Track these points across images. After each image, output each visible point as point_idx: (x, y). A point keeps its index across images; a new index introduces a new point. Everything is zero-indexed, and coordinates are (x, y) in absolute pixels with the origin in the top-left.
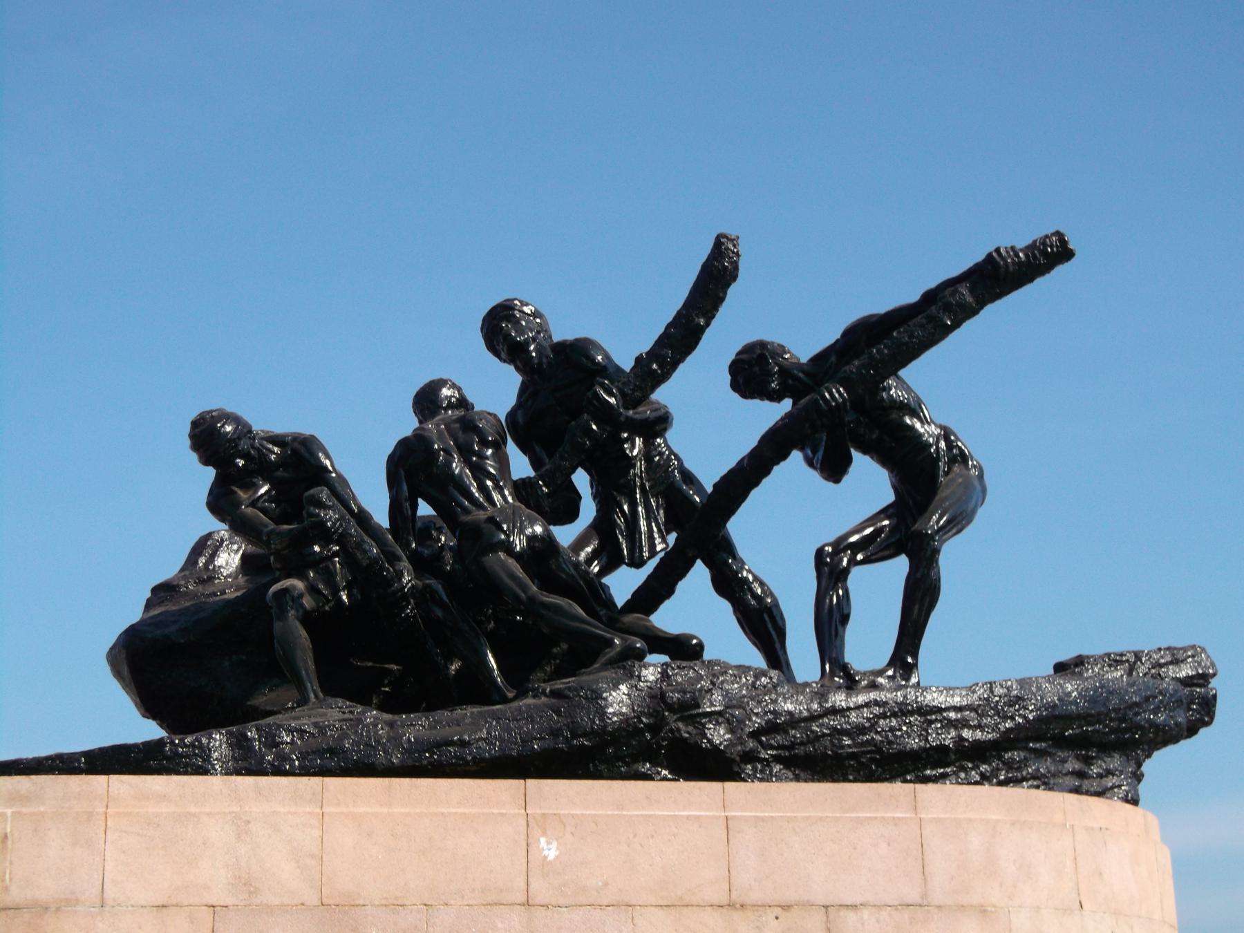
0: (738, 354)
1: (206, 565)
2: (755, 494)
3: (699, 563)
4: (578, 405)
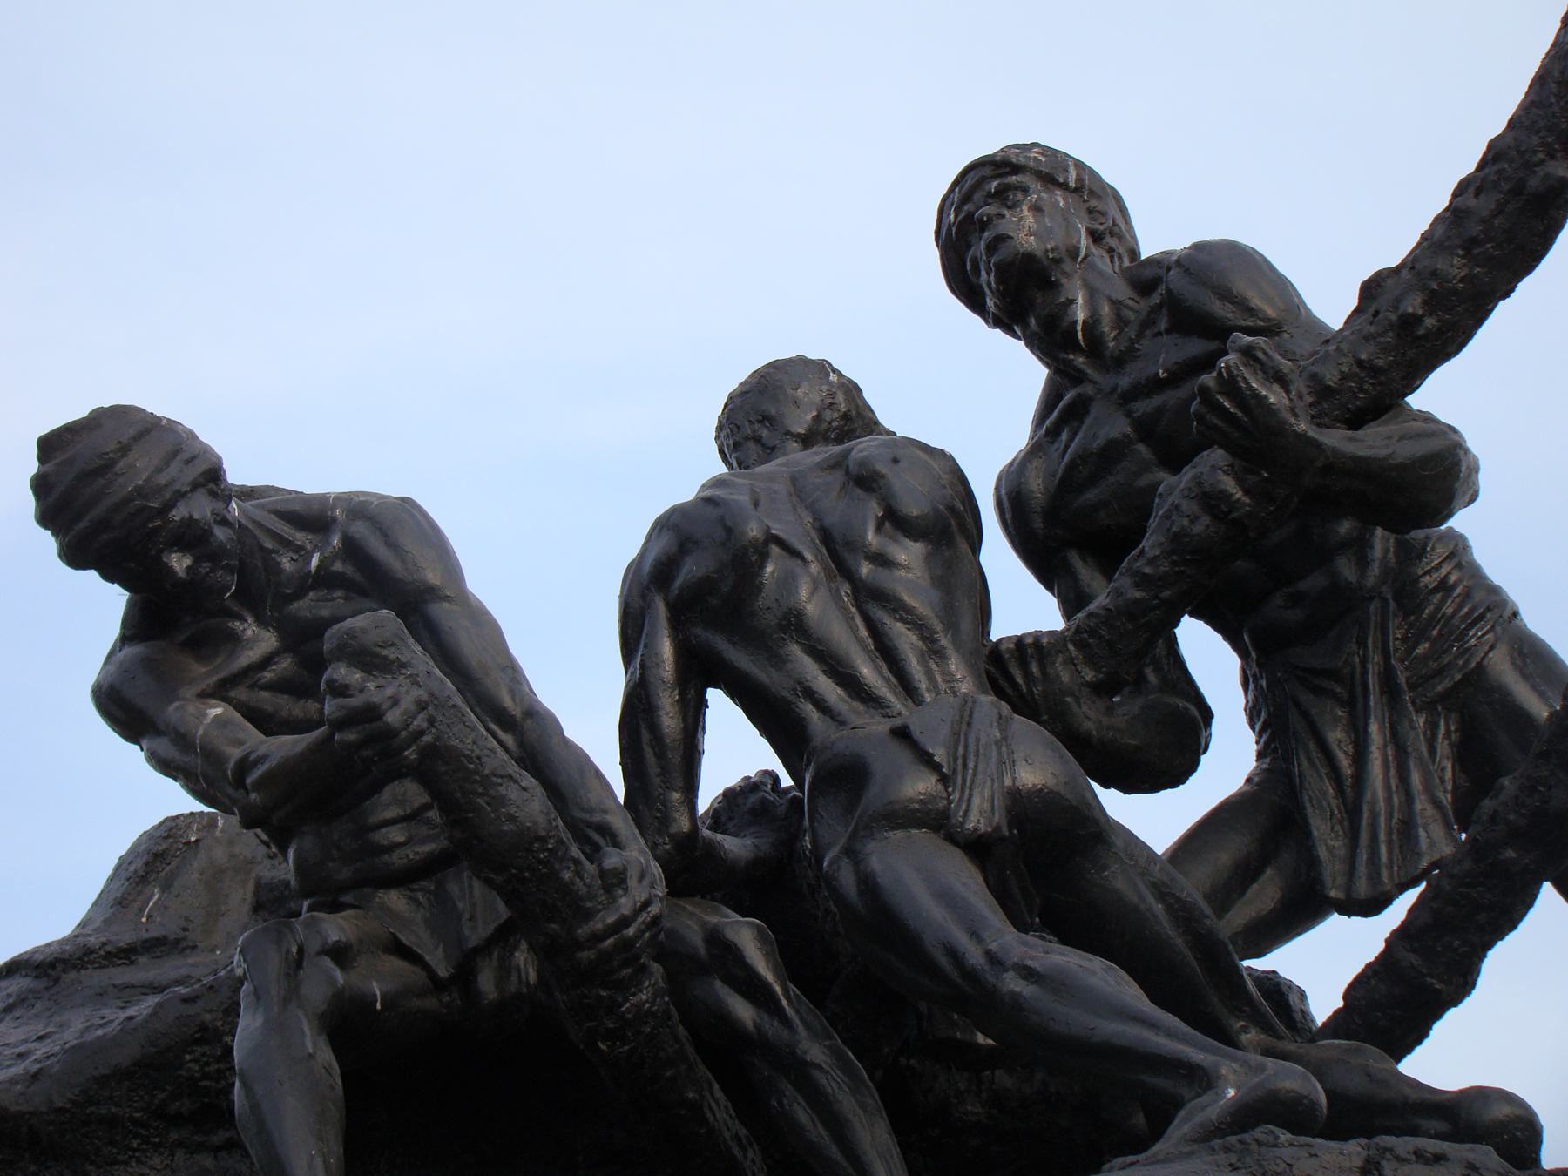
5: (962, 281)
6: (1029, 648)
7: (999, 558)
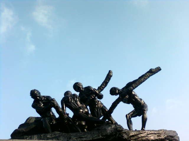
1: (29, 122)
4: (89, 95)
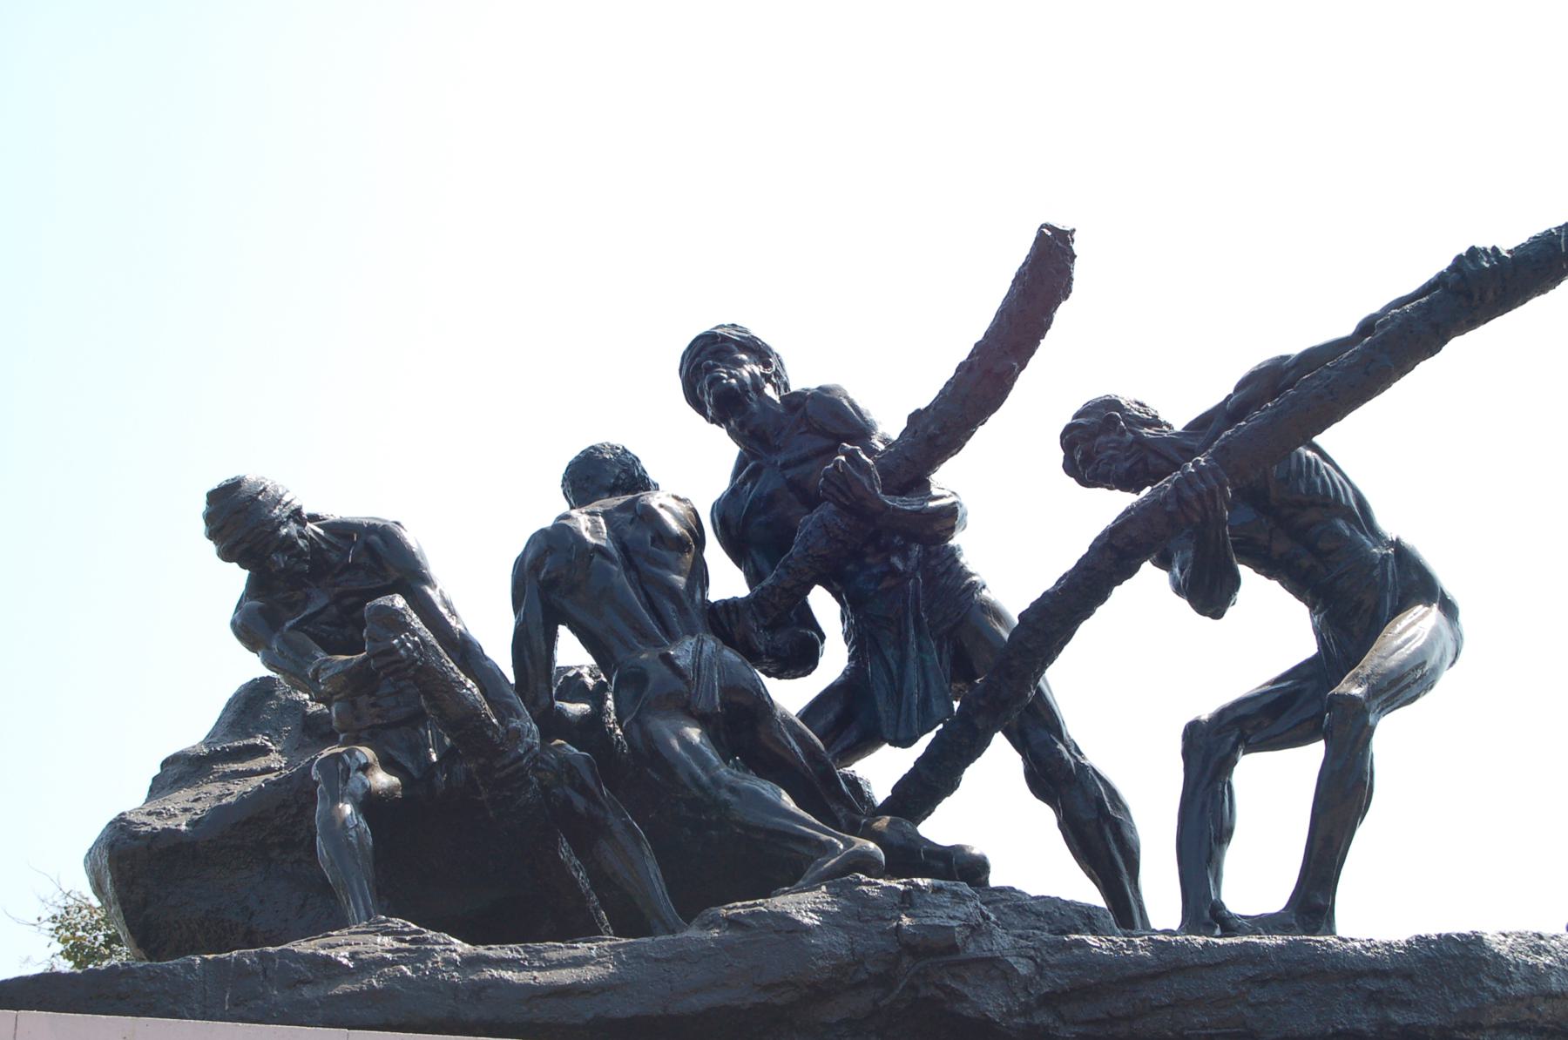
0: (1077, 416)
2: (1085, 628)
3: (999, 741)
4: (833, 495)
5: (694, 398)
6: (730, 606)
7: (715, 555)
